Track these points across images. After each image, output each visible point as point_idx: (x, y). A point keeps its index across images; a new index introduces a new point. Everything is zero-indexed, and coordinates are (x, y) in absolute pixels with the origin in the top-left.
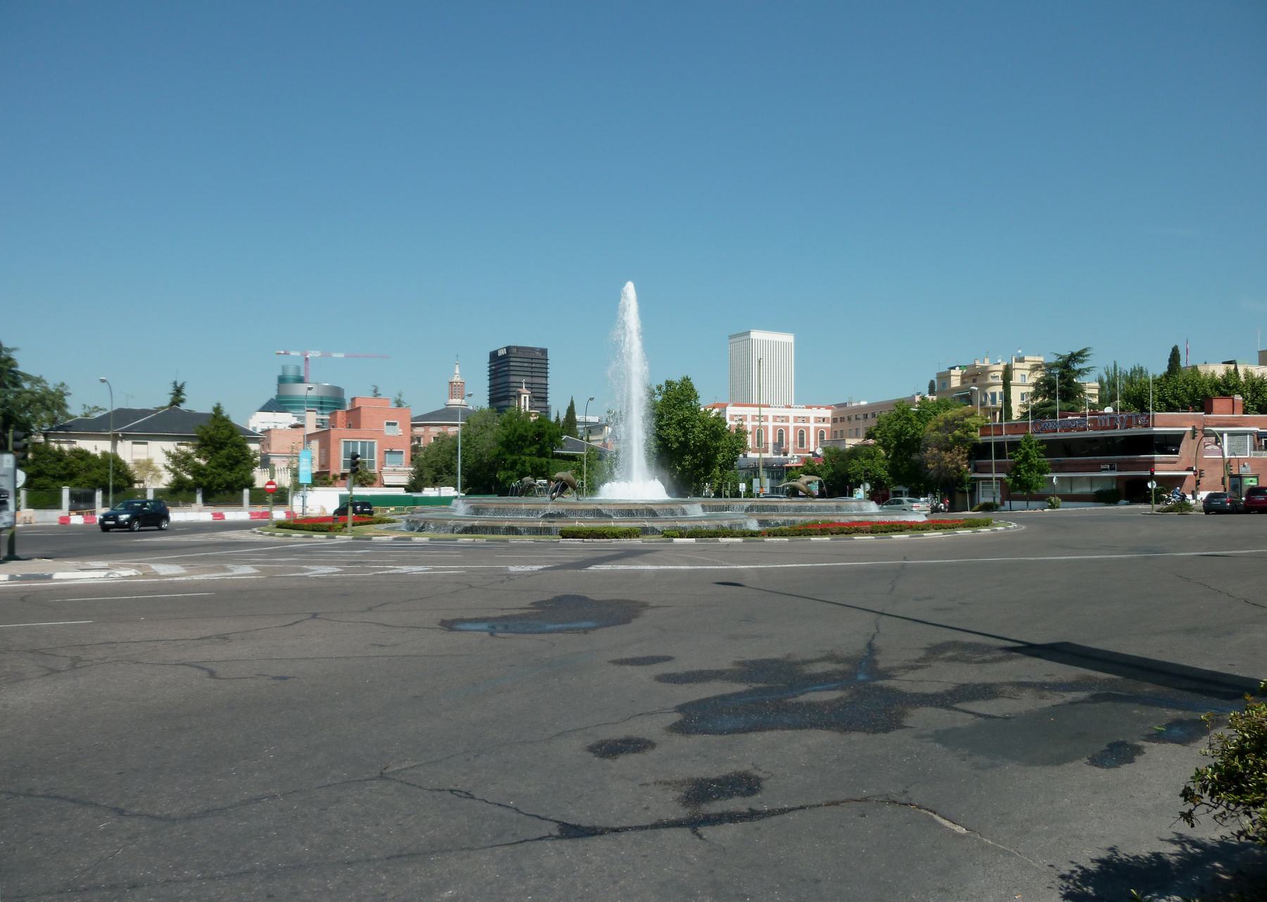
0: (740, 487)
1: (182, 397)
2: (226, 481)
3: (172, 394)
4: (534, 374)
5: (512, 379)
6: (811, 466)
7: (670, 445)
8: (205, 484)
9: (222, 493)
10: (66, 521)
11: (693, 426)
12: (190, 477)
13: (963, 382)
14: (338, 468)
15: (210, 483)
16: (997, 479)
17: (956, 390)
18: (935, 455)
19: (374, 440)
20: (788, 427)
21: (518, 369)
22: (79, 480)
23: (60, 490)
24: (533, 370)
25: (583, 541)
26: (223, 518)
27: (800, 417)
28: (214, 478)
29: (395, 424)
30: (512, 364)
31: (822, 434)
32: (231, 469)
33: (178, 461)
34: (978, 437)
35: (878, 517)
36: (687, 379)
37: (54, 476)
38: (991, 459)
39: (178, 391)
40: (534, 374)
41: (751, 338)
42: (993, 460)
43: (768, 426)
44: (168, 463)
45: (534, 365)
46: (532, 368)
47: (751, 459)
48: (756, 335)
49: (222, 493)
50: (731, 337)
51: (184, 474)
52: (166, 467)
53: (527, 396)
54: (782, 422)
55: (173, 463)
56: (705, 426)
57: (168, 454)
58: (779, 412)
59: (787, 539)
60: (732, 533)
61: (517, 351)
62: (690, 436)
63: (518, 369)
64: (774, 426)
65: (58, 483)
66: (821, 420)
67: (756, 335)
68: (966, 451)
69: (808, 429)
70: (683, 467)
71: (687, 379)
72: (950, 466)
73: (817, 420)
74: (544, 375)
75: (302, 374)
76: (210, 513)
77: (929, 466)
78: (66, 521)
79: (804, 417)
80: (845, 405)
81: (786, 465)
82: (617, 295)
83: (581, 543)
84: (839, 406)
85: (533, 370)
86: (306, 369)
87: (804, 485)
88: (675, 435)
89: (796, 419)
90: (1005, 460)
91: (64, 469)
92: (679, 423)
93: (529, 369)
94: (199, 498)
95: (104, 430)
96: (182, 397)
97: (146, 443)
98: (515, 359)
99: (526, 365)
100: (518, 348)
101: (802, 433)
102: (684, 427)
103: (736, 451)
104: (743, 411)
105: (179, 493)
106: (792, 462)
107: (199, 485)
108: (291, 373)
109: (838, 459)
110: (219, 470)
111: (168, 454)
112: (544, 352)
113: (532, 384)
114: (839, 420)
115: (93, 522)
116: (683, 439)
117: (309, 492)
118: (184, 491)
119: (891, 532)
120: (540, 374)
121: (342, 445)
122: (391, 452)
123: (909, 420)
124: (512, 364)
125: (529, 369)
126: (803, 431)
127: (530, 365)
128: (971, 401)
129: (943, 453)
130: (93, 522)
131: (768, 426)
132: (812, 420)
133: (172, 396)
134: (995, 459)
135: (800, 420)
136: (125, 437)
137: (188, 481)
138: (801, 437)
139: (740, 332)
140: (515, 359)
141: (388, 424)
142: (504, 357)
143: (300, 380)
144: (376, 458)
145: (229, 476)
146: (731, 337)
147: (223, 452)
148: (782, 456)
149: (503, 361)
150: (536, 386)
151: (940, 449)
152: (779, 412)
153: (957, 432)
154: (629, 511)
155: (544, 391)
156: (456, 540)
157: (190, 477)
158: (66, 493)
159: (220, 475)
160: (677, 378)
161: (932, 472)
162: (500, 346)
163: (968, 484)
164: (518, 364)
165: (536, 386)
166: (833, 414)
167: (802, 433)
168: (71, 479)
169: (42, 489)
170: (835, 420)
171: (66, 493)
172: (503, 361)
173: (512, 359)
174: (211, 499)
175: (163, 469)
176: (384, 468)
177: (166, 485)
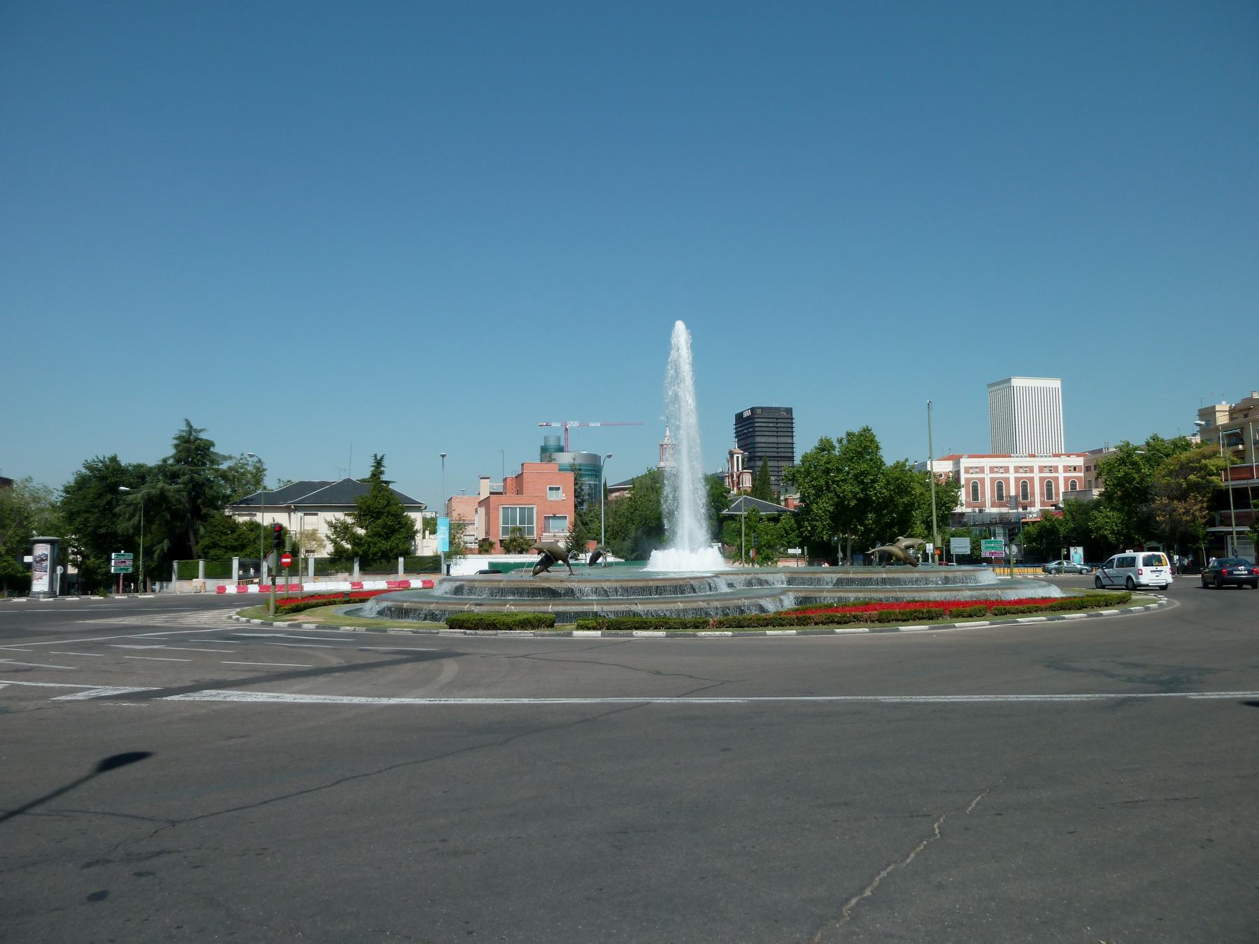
0: (927, 548)
1: (382, 469)
2: (380, 550)
3: (373, 466)
4: (779, 434)
5: (758, 439)
6: (1050, 520)
7: (846, 502)
8: (361, 553)
9: (378, 561)
10: (222, 591)
11: (873, 481)
12: (349, 546)
13: (1232, 418)
14: (498, 535)
15: (365, 553)
16: (1238, 533)
17: (1224, 427)
18: (1166, 506)
19: (532, 506)
20: (1033, 477)
21: (763, 429)
22: (248, 550)
23: (231, 560)
24: (779, 430)
25: (465, 633)
26: (362, 588)
27: (1046, 467)
28: (370, 546)
29: (558, 489)
30: (756, 425)
31: (1073, 485)
32: (387, 538)
33: (341, 530)
34: (1220, 481)
35: (936, 593)
36: (868, 430)
37: (226, 547)
38: (1230, 509)
39: (379, 463)
40: (779, 434)
41: (1013, 385)
42: (1233, 511)
43: (1009, 478)
44: (329, 533)
45: (779, 425)
46: (777, 427)
47: (990, 514)
48: (1017, 382)
49: (378, 561)
50: (990, 385)
51: (343, 543)
52: (328, 537)
53: (740, 456)
54: (1026, 472)
55: (335, 532)
56: (888, 481)
57: (330, 525)
58: (1022, 462)
59: (730, 633)
60: (666, 623)
61: (762, 412)
62: (871, 492)
63: (763, 429)
64: (1015, 478)
65: (229, 554)
66: (1072, 469)
67: (1017, 382)
68: (1205, 499)
69: (1056, 479)
70: (865, 526)
71: (867, 430)
72: (1185, 518)
73: (1067, 469)
74: (790, 434)
75: (562, 444)
76: (384, 582)
77: (1158, 518)
78: (222, 591)
79: (1051, 467)
80: (1100, 451)
81: (1023, 520)
82: (665, 344)
83: (463, 636)
84: (1093, 452)
85: (779, 430)
86: (566, 439)
87: (901, 550)
88: (852, 492)
89: (1041, 469)
90: (1249, 510)
91: (236, 540)
92: (856, 477)
93: (775, 429)
94: (356, 567)
95: (281, 502)
96: (382, 469)
97: (316, 514)
98: (759, 420)
99: (771, 425)
100: (763, 409)
101: (1049, 485)
102: (862, 482)
103: (946, 507)
104: (1075, 462)
105: (338, 562)
106: (1031, 516)
107: (356, 554)
108: (552, 443)
109: (1080, 512)
110: (376, 539)
111: (330, 525)
112: (789, 411)
113: (778, 444)
114: (1093, 468)
115: (245, 592)
116: (862, 495)
117: (462, 560)
118: (343, 560)
119: (914, 620)
120: (786, 434)
121: (501, 511)
122: (554, 517)
123: (1134, 464)
124: (756, 425)
125: (775, 429)
126: (1075, 482)
127: (775, 425)
128: (1242, 440)
129: (1175, 502)
130: (245, 592)
131: (1009, 478)
132: (1061, 469)
133: (373, 468)
134: (1234, 509)
135: (1047, 470)
136: (297, 509)
137: (346, 551)
138: (1049, 488)
139: (1000, 380)
140: (759, 420)
141: (551, 489)
142: (749, 418)
143: (561, 449)
144: (535, 525)
145: (384, 545)
146: (990, 385)
147: (379, 521)
148: (1020, 510)
149: (749, 422)
150: (782, 445)
151: (1171, 499)
152: (1022, 462)
153: (1192, 477)
154: (681, 587)
155: (790, 450)
156: (338, 628)
157: (349, 546)
158: (235, 563)
159: (375, 544)
160: (856, 429)
161: (1164, 525)
162: (744, 407)
163: (1204, 540)
164: (763, 425)
165: (782, 445)
166: (1085, 462)
167: (1049, 485)
168: (242, 550)
169: (215, 560)
170: (1088, 469)
171: (235, 563)
172: (749, 422)
173: (756, 420)
174: (367, 568)
175: (325, 539)
176: (544, 534)
177: (330, 555)
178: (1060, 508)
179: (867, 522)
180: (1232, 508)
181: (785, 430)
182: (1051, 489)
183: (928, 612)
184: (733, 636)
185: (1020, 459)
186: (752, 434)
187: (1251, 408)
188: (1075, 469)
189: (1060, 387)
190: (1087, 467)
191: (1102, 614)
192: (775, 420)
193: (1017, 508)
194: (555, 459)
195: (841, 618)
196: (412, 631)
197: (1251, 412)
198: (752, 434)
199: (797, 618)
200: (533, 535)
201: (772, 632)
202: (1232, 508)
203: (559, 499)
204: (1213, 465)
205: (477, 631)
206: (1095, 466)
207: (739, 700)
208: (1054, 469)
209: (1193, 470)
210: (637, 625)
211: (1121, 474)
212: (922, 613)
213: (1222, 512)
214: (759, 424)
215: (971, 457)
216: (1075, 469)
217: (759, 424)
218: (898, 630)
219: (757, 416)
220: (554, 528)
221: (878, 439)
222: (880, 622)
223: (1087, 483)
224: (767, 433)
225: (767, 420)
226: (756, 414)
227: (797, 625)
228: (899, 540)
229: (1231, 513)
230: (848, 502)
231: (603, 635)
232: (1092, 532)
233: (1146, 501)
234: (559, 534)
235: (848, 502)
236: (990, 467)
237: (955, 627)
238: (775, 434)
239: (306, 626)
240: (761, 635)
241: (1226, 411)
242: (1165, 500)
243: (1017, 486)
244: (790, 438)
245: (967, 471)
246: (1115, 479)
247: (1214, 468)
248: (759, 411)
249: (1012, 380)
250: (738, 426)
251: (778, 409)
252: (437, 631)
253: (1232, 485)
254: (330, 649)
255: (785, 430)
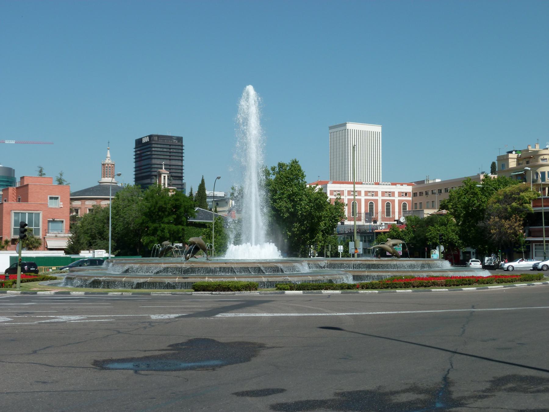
0: (339, 249)
4: (172, 158)
6: (396, 231)
7: (282, 215)
11: (301, 200)
13: (518, 164)
14: (9, 234)
18: (496, 223)
21: (159, 153)
24: (171, 154)
25: (212, 294)
27: (386, 192)
29: (57, 198)
31: (405, 206)
34: (530, 207)
38: (543, 226)
40: (172, 158)
42: (544, 227)
45: (171, 150)
46: (170, 152)
48: (351, 126)
50: (331, 128)
53: (166, 176)
56: (310, 200)
62: (298, 207)
63: (159, 153)
64: (399, 200)
66: (404, 194)
67: (351, 126)
68: (522, 219)
69: (393, 201)
71: (295, 162)
72: (509, 231)
74: (180, 158)
77: (492, 231)
79: (390, 192)
80: (423, 182)
81: (376, 231)
83: (210, 295)
84: (418, 183)
85: (171, 154)
88: (286, 207)
89: (383, 193)
92: (289, 197)
93: (168, 154)
99: (165, 150)
100: (159, 136)
101: (388, 205)
102: (293, 201)
103: (335, 220)
106: (381, 228)
112: (180, 139)
116: (292, 210)
120: (177, 158)
121: (13, 215)
122: (54, 221)
123: (475, 194)
125: (168, 154)
127: (168, 150)
129: (503, 221)
132: (396, 194)
141: (51, 198)
142: (147, 143)
146: (331, 128)
148: (372, 223)
150: (174, 167)
151: (501, 218)
153: (514, 204)
160: (287, 161)
162: (144, 134)
163: (523, 246)
164: (159, 149)
165: (174, 167)
167: (388, 205)
170: (415, 195)
173: (154, 145)
178: (402, 223)
179: (293, 229)
180: (544, 225)
181: (177, 154)
182: (390, 209)
183: (468, 281)
184: (378, 293)
185: (368, 186)
186: (149, 156)
187: (531, 157)
188: (406, 194)
189: (380, 131)
190: (414, 193)
191: (548, 283)
192: (168, 146)
193: (370, 222)
194: (44, 174)
195: (427, 283)
196: (171, 293)
197: (531, 160)
198: (149, 156)
199: (404, 283)
200: (39, 235)
201: (399, 291)
202: (544, 225)
203: (57, 207)
204: (527, 197)
205: (221, 292)
206: (420, 192)
207: (513, 309)
208: (391, 194)
209: (515, 199)
210: (315, 288)
211: (466, 200)
212: (466, 281)
213: (531, 227)
214: (156, 149)
215: (334, 183)
216: (406, 194)
217: (156, 149)
218: (462, 290)
219: (153, 142)
220: (53, 230)
221: (303, 169)
222: (445, 286)
223: (414, 204)
224: (162, 157)
225: (162, 146)
226: (153, 140)
227: (404, 288)
228: (388, 240)
229: (543, 228)
230: (283, 215)
231: (304, 293)
232: (428, 241)
233: (483, 219)
234: (60, 235)
235: (283, 215)
236: (348, 191)
237: (488, 288)
238: (168, 157)
239: (39, 293)
240: (394, 292)
241: (514, 158)
242: (497, 219)
243: (366, 206)
244: (180, 161)
245: (332, 193)
246: (463, 203)
247: (527, 199)
248: (156, 138)
249: (347, 124)
250: (139, 149)
251: (171, 138)
252: (191, 293)
253: (544, 210)
254: (56, 312)
255: (177, 154)
